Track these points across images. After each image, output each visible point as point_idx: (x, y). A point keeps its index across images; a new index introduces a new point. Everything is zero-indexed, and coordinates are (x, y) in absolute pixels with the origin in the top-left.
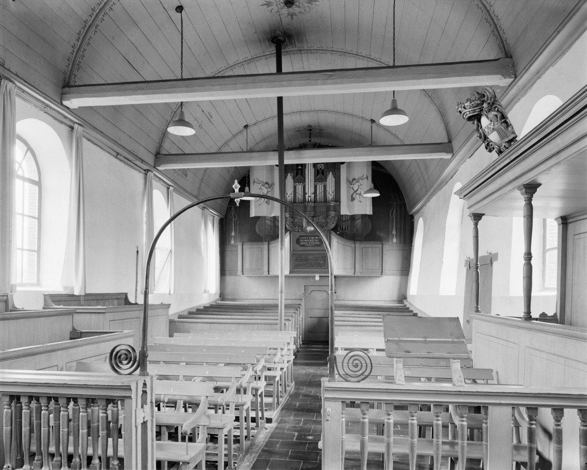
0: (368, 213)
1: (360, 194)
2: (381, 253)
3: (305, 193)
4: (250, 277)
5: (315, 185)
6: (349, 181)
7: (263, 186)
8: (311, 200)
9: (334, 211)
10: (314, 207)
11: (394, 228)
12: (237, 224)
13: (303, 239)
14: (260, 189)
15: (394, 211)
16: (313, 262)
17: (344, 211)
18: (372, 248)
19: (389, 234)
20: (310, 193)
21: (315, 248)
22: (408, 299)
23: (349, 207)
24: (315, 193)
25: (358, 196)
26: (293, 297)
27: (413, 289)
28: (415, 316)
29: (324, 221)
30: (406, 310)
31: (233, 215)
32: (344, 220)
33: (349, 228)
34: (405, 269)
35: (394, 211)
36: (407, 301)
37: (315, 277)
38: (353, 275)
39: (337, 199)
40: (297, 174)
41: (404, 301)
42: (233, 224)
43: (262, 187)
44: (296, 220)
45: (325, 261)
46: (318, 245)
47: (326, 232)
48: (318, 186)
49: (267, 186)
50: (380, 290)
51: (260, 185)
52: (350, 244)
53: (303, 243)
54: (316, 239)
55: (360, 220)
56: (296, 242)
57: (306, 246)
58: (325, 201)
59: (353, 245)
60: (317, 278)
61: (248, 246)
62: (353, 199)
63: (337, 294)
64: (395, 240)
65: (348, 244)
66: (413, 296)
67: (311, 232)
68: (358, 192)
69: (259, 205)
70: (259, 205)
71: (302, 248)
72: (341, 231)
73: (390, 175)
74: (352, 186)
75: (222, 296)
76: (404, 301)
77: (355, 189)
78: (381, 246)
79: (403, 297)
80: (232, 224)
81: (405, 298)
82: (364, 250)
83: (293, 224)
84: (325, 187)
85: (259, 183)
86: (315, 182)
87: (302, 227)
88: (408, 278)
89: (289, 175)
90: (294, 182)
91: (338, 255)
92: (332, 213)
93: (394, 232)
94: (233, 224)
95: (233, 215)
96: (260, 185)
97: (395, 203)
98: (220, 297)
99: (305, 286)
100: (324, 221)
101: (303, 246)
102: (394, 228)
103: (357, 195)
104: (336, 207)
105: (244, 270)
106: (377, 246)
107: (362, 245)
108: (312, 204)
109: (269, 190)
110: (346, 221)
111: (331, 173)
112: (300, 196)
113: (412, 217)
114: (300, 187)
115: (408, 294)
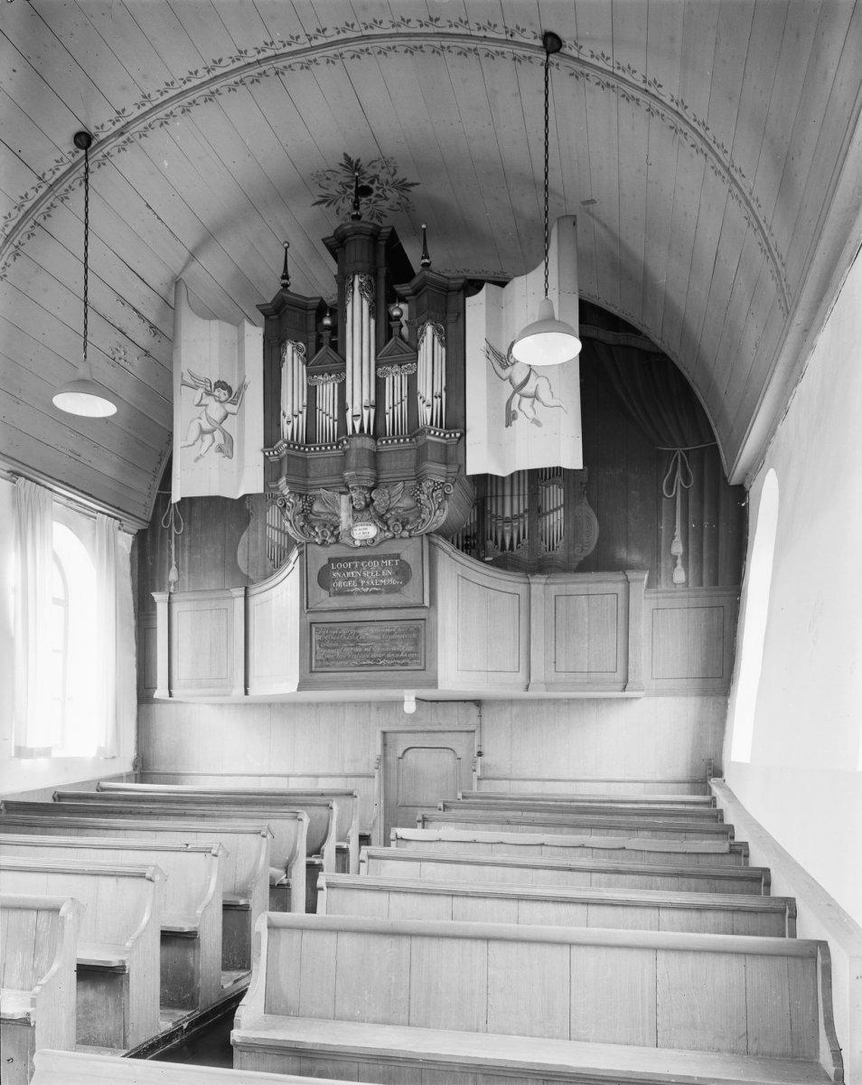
0: (567, 465)
1: (535, 396)
2: (621, 612)
3: (343, 408)
4: (221, 705)
5: (377, 378)
6: (497, 355)
7: (209, 394)
8: (362, 429)
9: (446, 463)
10: (375, 456)
11: (678, 533)
12: (184, 545)
13: (342, 571)
14: (198, 405)
15: (678, 474)
16: (377, 648)
17: (478, 462)
18: (592, 595)
19: (658, 553)
20: (357, 404)
21: (384, 599)
22: (726, 776)
23: (497, 446)
24: (378, 404)
25: (526, 402)
26: (348, 769)
27: (739, 748)
28: (739, 853)
29: (407, 502)
30: (714, 822)
31: (172, 518)
32: (508, 514)
33: (526, 541)
34: (717, 672)
35: (678, 474)
36: (723, 786)
37: (401, 702)
38: (519, 693)
39: (454, 420)
40: (319, 346)
41: (713, 782)
42: (173, 547)
43: (207, 400)
44: (317, 507)
45: (416, 642)
46: (391, 589)
47: (417, 541)
48: (388, 381)
49: (222, 394)
50: (627, 746)
51: (201, 391)
52: (509, 583)
53: (340, 584)
54: (384, 567)
55: (560, 513)
56: (320, 579)
57: (350, 593)
58: (414, 429)
59: (521, 589)
60: (410, 707)
61: (187, 606)
62: (510, 417)
63: (486, 759)
64: (679, 576)
65: (503, 586)
66: (739, 764)
67: (366, 544)
68: (528, 389)
69: (197, 459)
70: (197, 459)
71: (336, 602)
72: (499, 553)
73: (664, 355)
74: (505, 374)
75: (143, 769)
76: (713, 782)
77: (518, 380)
78: (620, 587)
79: (708, 771)
80: (170, 545)
81: (718, 773)
82: (561, 607)
83: (306, 518)
84: (412, 380)
85: (195, 388)
86: (377, 366)
87: (336, 528)
88: (726, 704)
89: (289, 348)
90: (309, 373)
91: (472, 627)
92: (436, 472)
93: (677, 548)
94: (173, 547)
95: (172, 518)
96: (201, 391)
97: (679, 451)
98: (135, 766)
99: (384, 733)
100: (407, 502)
101: (340, 593)
102: (678, 533)
103: (524, 400)
104: (451, 451)
105: (175, 683)
106: (606, 586)
107: (554, 589)
108: (368, 443)
109: (230, 407)
110: (514, 518)
111: (429, 329)
112: (327, 421)
113: (741, 492)
114: (327, 391)
115: (725, 759)
